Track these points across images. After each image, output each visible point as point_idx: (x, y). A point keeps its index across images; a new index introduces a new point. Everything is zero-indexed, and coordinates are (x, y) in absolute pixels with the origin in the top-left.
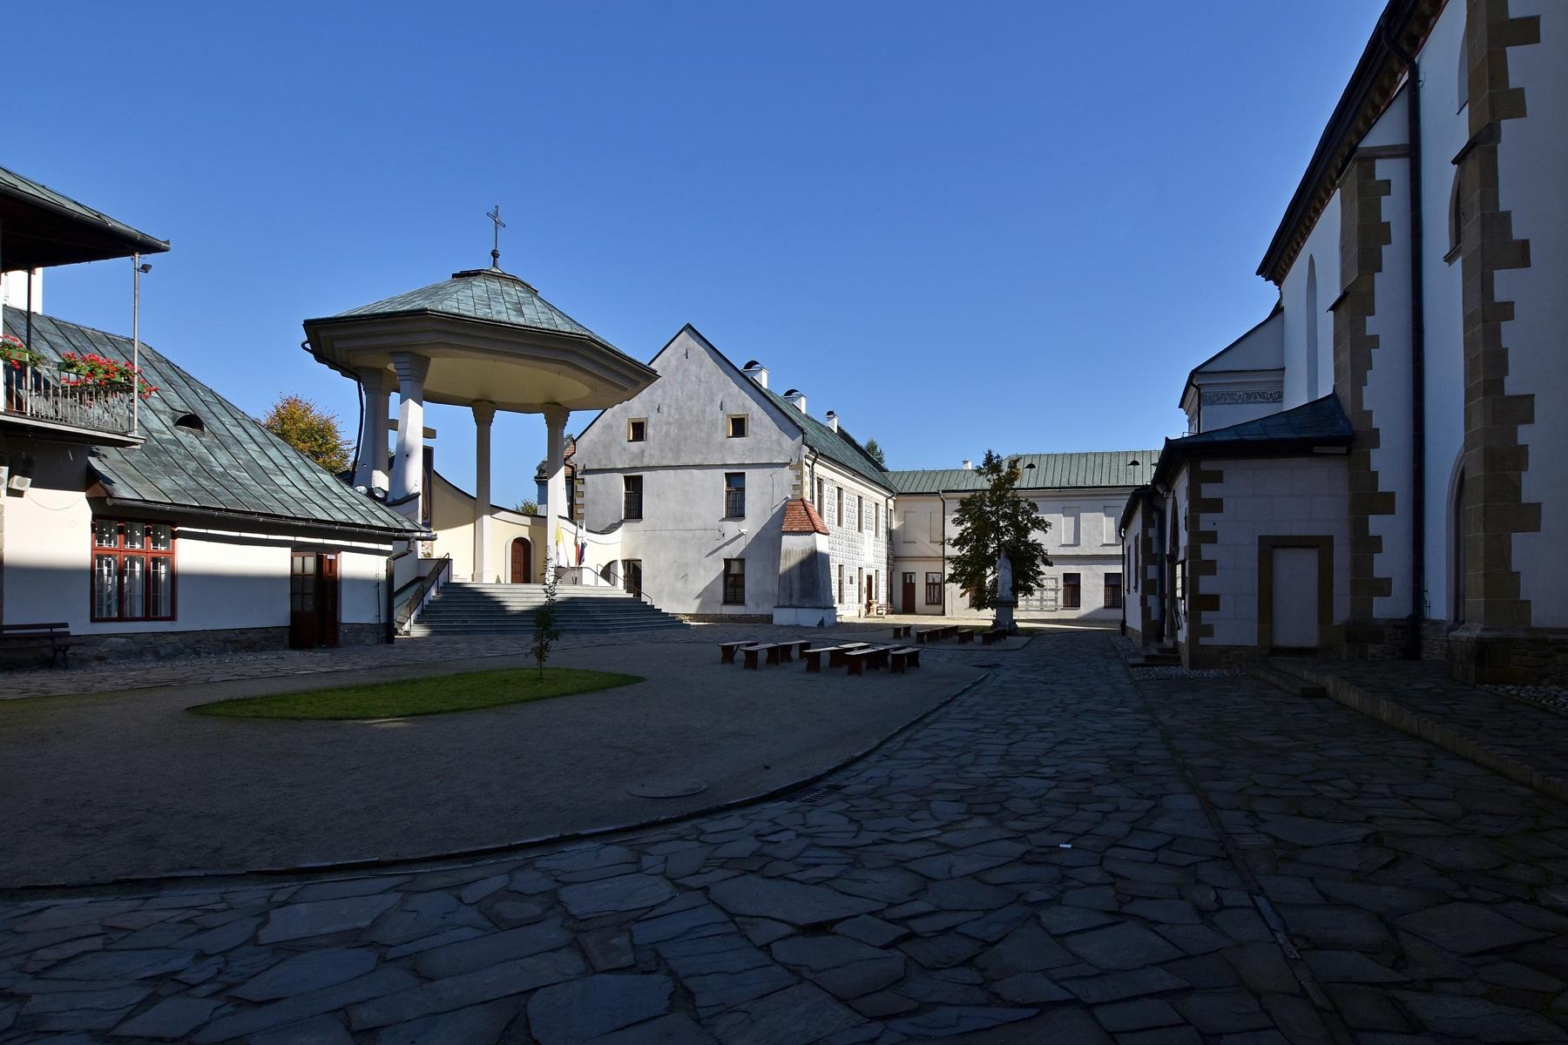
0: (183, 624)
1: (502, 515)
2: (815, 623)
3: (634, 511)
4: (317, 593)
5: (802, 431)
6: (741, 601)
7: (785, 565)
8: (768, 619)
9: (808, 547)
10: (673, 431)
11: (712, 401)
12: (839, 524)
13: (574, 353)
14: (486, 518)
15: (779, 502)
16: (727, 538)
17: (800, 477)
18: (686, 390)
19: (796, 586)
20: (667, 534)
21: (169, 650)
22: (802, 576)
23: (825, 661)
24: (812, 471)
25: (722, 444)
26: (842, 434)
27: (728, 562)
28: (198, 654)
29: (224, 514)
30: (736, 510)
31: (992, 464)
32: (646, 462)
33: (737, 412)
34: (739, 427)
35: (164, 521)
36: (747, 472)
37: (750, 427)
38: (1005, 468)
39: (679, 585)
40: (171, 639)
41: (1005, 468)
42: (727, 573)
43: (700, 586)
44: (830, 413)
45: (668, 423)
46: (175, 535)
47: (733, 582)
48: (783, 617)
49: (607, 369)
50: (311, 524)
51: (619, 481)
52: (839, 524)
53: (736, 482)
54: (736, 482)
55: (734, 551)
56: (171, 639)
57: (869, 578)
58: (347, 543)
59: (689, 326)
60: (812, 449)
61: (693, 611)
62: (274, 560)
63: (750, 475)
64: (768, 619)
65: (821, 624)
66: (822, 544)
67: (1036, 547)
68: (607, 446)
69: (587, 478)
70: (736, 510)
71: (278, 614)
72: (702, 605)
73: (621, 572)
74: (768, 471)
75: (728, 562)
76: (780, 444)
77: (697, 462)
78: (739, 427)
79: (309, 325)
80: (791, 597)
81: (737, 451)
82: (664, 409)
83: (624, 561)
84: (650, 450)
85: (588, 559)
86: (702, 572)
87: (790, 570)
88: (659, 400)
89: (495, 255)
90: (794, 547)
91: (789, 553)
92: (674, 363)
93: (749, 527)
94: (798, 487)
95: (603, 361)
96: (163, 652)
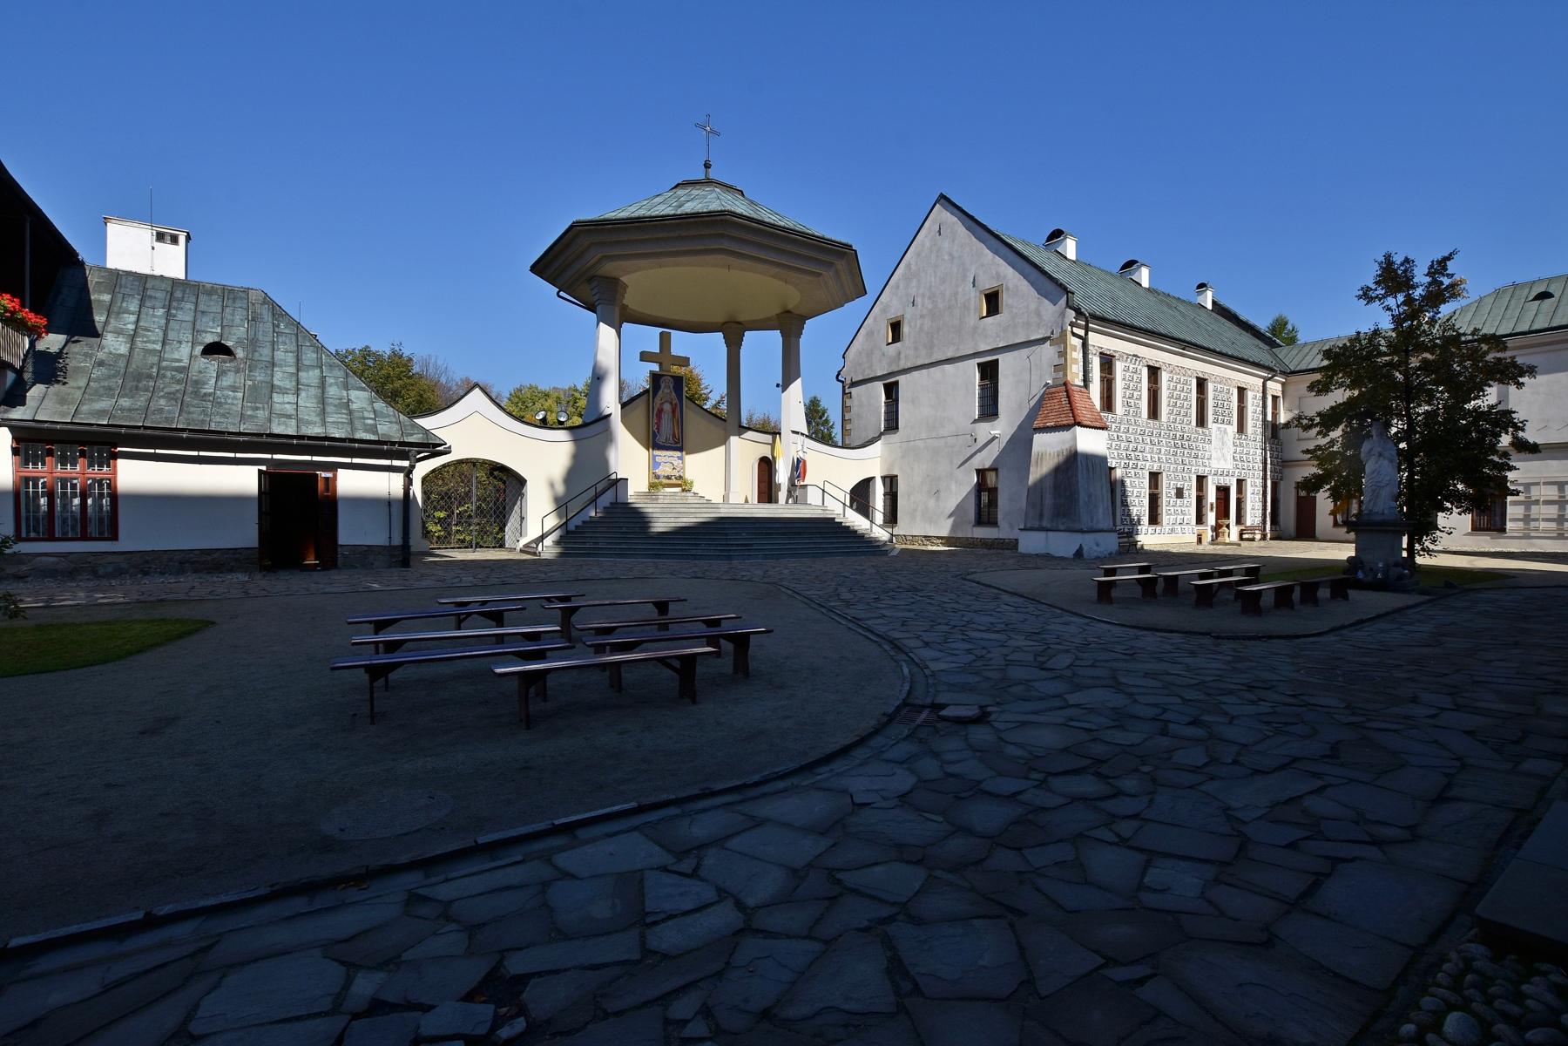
0: (125, 543)
1: (750, 434)
2: (1070, 553)
3: (892, 425)
4: (296, 510)
5: (1065, 290)
6: (993, 523)
7: (1036, 473)
8: (1014, 544)
9: (1067, 446)
10: (927, 323)
11: (965, 277)
12: (1154, 413)
13: (722, 236)
14: (734, 440)
15: (1037, 391)
16: (980, 443)
17: (1063, 354)
18: (930, 271)
19: (1048, 501)
20: (921, 444)
21: (110, 569)
22: (1056, 487)
23: (1267, 601)
24: (1085, 345)
25: (975, 328)
26: (1219, 309)
27: (981, 473)
28: (146, 574)
29: (142, 431)
30: (989, 410)
31: (1393, 278)
32: (903, 364)
33: (988, 284)
34: (993, 301)
35: (105, 443)
36: (1000, 357)
37: (1005, 300)
38: (1420, 277)
39: (932, 503)
40: (110, 559)
41: (1420, 277)
42: (981, 487)
43: (952, 502)
44: (1202, 286)
45: (922, 316)
46: (115, 456)
47: (985, 493)
48: (1032, 543)
49: (761, 246)
50: (264, 439)
51: (879, 389)
52: (1154, 413)
53: (989, 372)
54: (989, 372)
55: (986, 459)
56: (110, 559)
57: (1223, 492)
58: (348, 460)
59: (942, 197)
60: (1079, 312)
61: (945, 533)
62: (243, 479)
63: (1006, 363)
64: (1014, 544)
65: (1079, 554)
66: (1089, 441)
67: (1503, 419)
68: (869, 355)
69: (854, 390)
70: (989, 410)
71: (247, 535)
72: (954, 527)
73: (879, 490)
74: (1024, 352)
75: (981, 473)
76: (1038, 314)
77: (950, 355)
78: (993, 301)
79: (540, 268)
80: (1041, 516)
81: (992, 333)
82: (919, 301)
83: (884, 478)
84: (907, 351)
85: (829, 481)
86: (953, 487)
87: (1042, 481)
88: (913, 291)
89: (707, 166)
90: (1048, 448)
91: (1041, 456)
92: (928, 244)
93: (1002, 428)
94: (1061, 368)
95: (766, 241)
96: (101, 571)
